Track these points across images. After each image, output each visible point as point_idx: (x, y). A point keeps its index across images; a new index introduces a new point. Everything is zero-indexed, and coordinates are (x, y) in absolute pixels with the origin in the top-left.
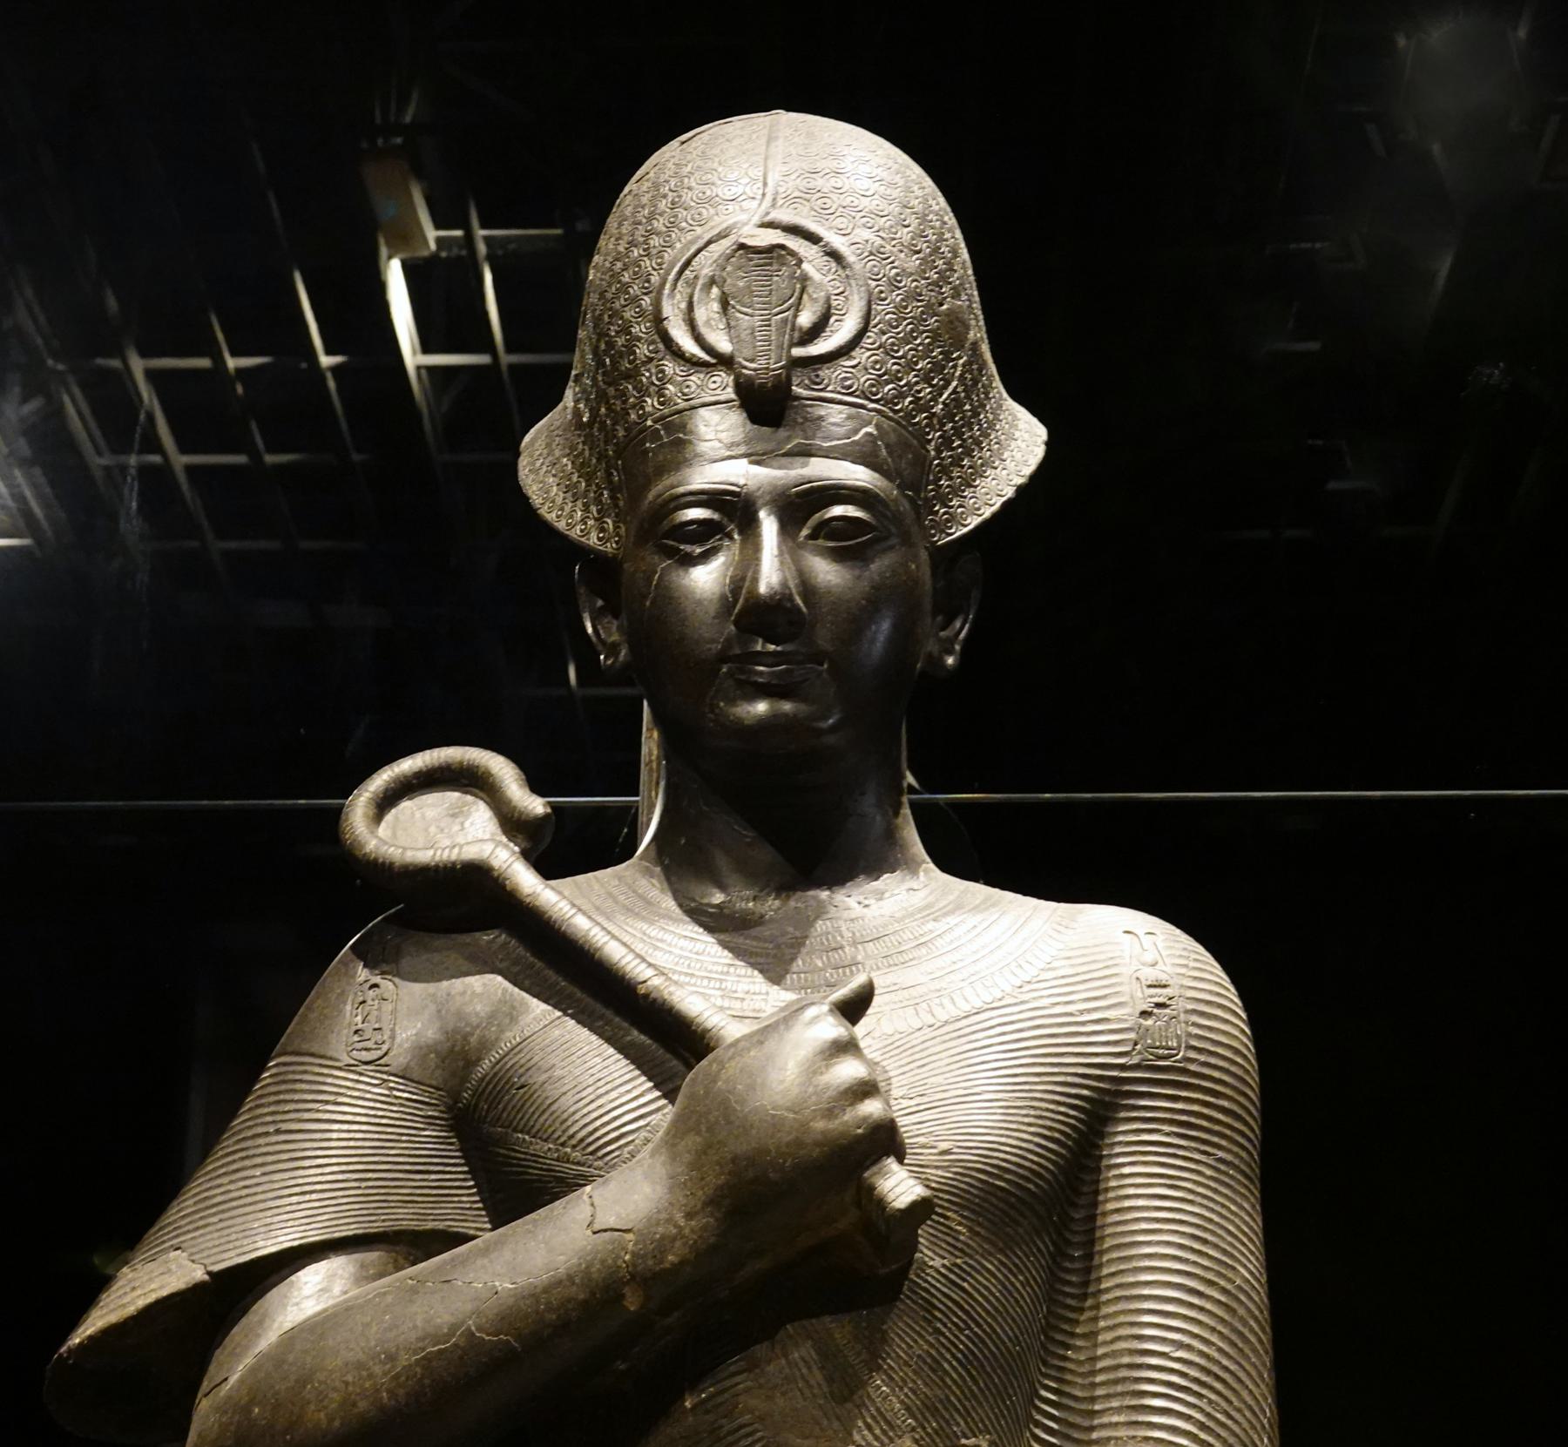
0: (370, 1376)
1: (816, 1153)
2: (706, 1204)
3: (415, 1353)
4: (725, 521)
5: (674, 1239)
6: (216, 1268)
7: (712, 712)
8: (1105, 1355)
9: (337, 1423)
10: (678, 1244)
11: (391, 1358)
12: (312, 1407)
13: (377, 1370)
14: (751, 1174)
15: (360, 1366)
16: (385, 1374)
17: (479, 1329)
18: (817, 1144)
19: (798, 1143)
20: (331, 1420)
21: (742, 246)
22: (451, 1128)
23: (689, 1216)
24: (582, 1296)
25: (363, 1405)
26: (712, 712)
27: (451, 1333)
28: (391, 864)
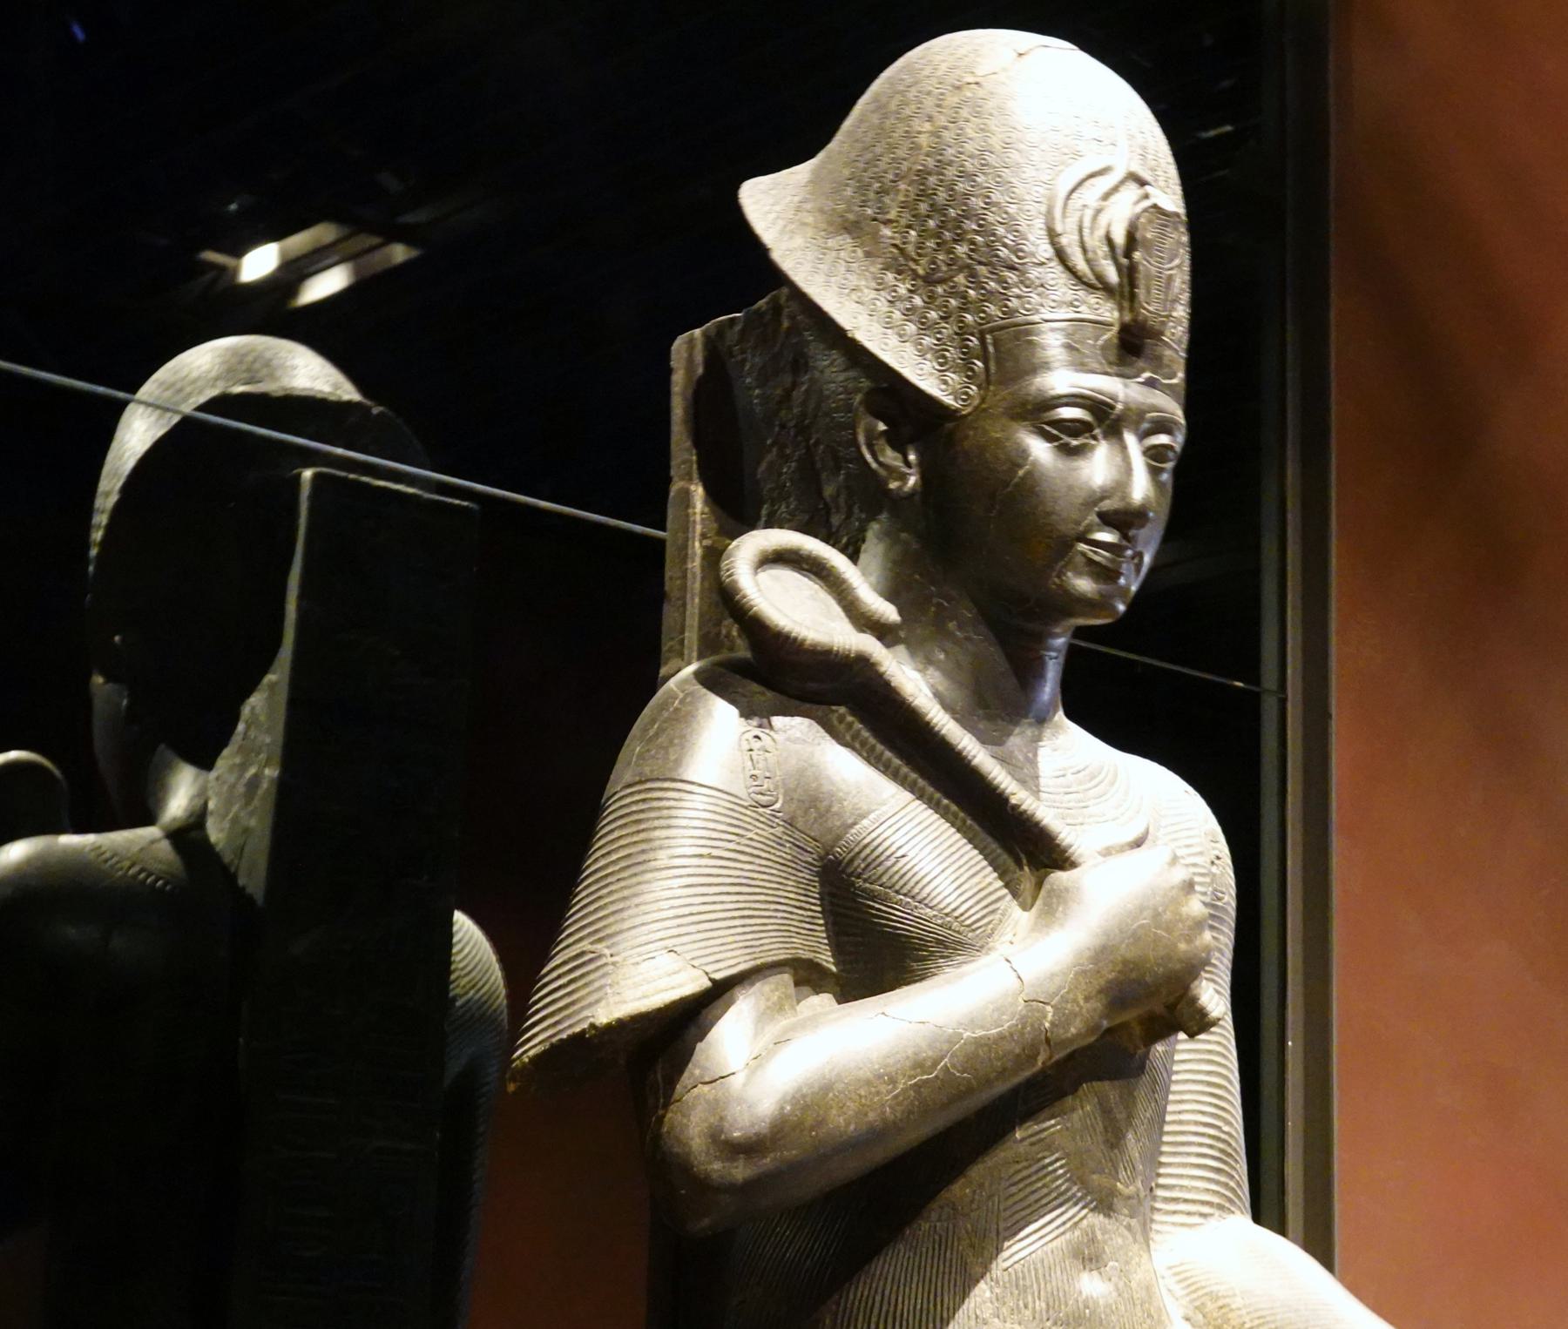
0: (878, 1093)
1: (1178, 966)
2: (1100, 992)
3: (911, 1077)
4: (1095, 424)
5: (1076, 1015)
6: (718, 976)
7: (1059, 577)
8: (1174, 1122)
9: (852, 1127)
10: (1078, 1020)
11: (893, 1081)
12: (834, 1112)
13: (883, 1088)
14: (1134, 975)
15: (868, 1083)
16: (889, 1092)
17: (954, 1066)
18: (1180, 961)
19: (1169, 958)
20: (848, 1125)
21: (1155, 206)
22: (818, 874)
23: (1087, 999)
24: (1017, 1051)
25: (872, 1116)
26: (1059, 577)
27: (935, 1063)
28: (804, 641)
